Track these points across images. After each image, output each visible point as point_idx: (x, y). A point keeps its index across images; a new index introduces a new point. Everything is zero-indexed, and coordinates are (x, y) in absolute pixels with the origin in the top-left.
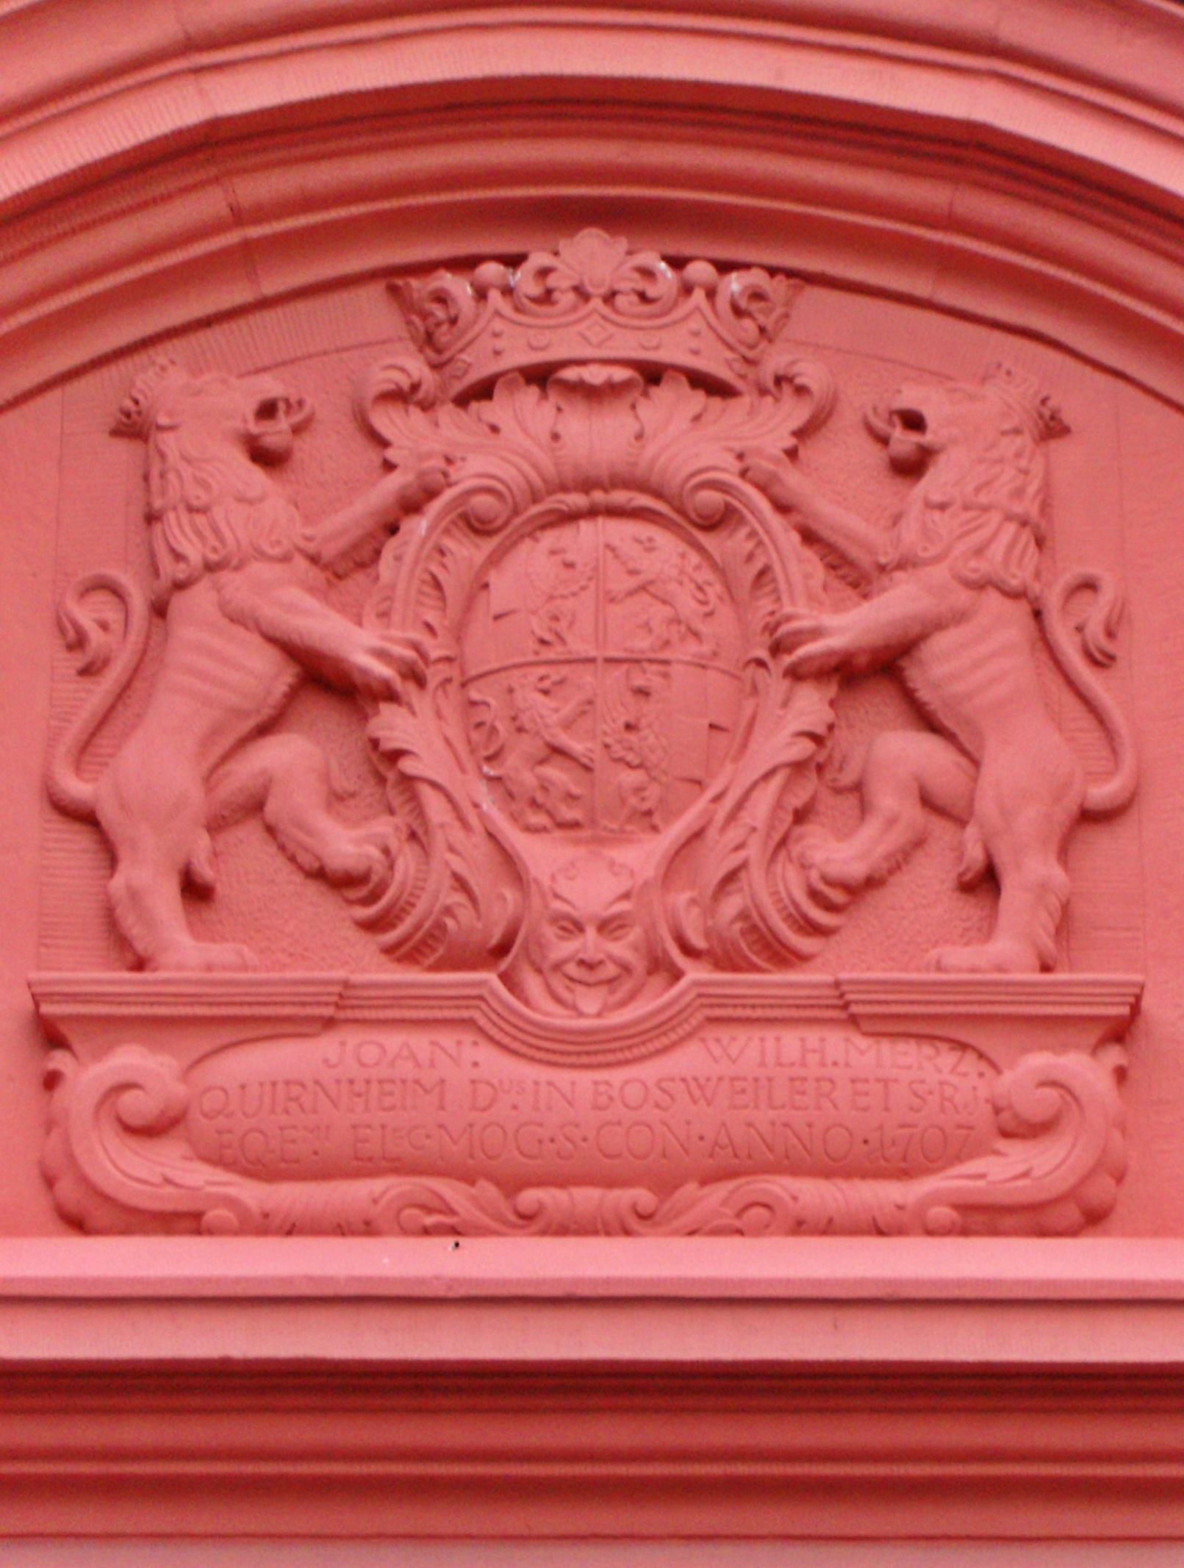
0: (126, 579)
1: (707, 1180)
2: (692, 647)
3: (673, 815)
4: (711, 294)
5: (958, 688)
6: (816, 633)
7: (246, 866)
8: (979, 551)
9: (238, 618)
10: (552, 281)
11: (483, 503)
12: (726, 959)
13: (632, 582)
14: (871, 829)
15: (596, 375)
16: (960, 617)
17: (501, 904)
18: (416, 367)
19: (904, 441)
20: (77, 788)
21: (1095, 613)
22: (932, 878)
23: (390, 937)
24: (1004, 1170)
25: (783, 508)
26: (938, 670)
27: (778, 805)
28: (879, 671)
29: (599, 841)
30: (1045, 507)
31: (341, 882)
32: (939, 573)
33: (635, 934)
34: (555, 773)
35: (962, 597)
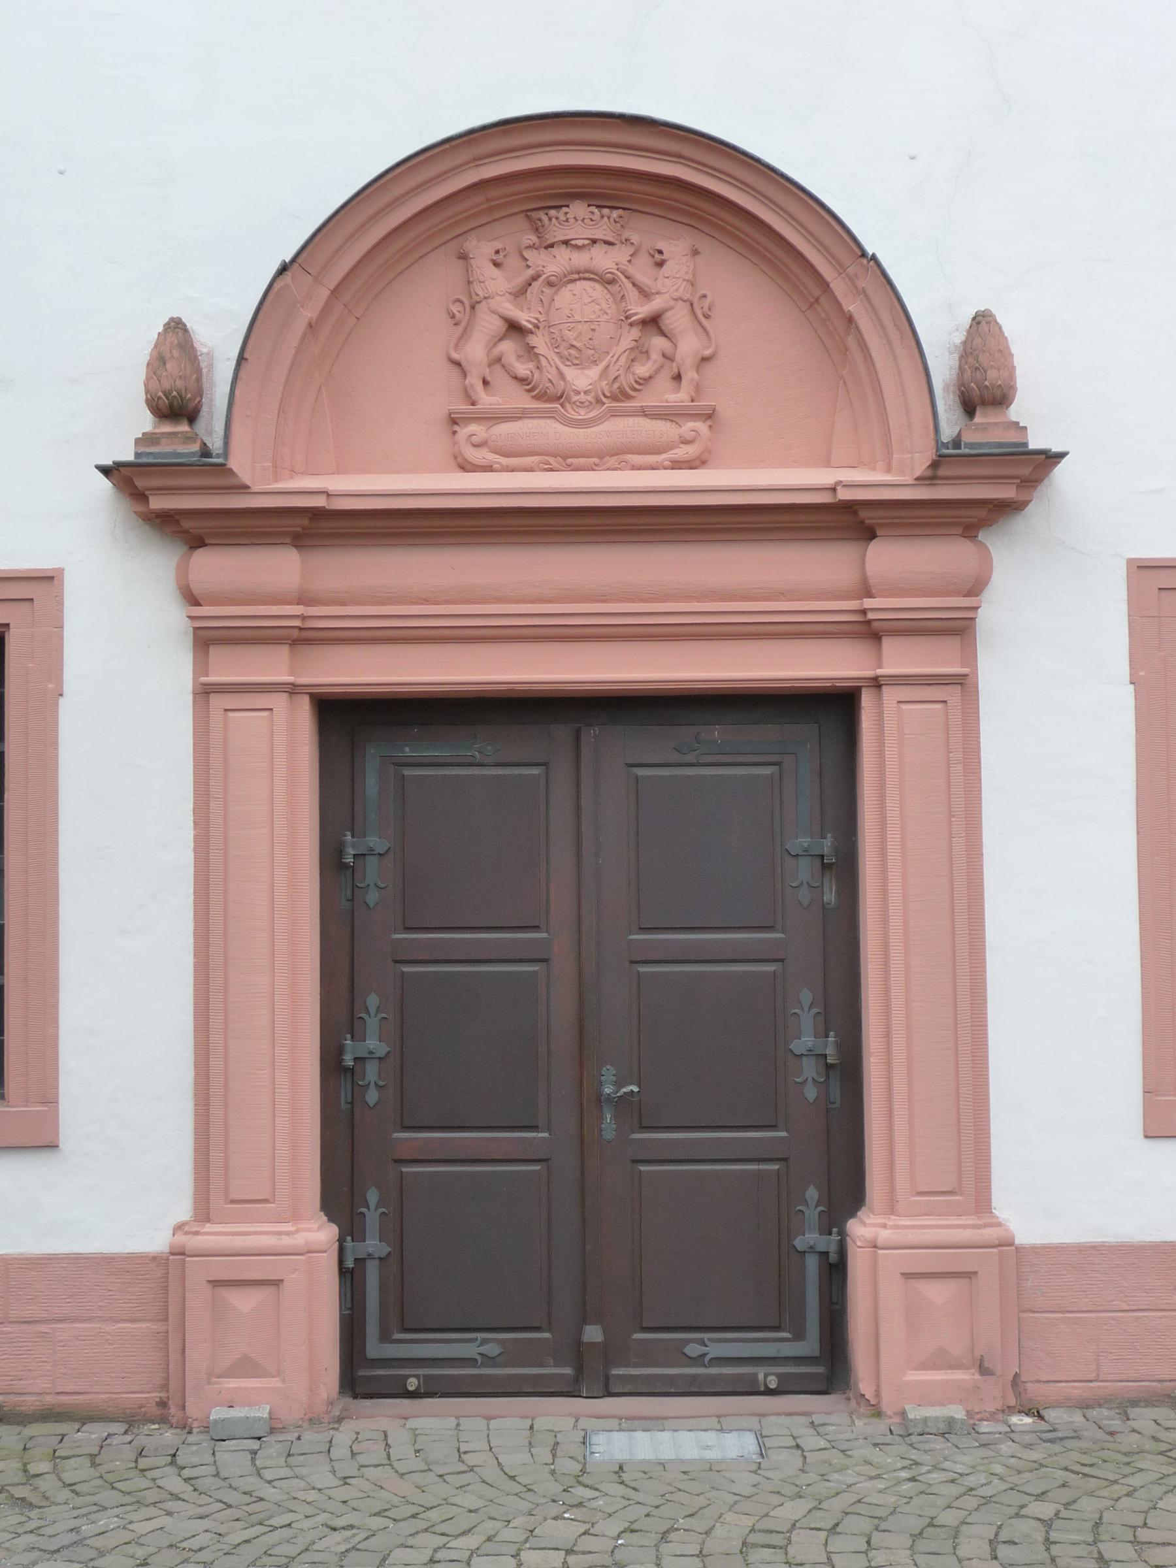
3: (601, 361)
6: (636, 314)
7: (498, 377)
8: (677, 290)
9: (493, 312)
12: (615, 398)
14: (649, 364)
15: (580, 243)
16: (671, 308)
17: (561, 385)
19: (658, 257)
20: (456, 356)
21: (706, 303)
22: (666, 375)
25: (627, 278)
26: (667, 322)
28: (653, 322)
30: (694, 275)
31: (522, 380)
32: (666, 297)
34: (572, 351)
35: (672, 303)
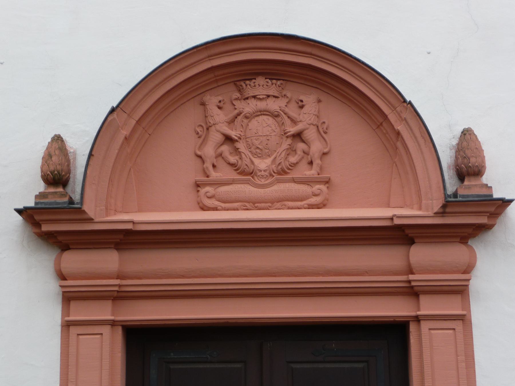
0: (203, 125)
1: (278, 202)
2: (274, 133)
3: (272, 155)
4: (276, 84)
5: (308, 138)
6: (290, 132)
7: (220, 163)
8: (310, 120)
10: (256, 84)
11: (248, 115)
12: (279, 173)
13: (266, 125)
14: (297, 156)
15: (261, 97)
16: (307, 129)
17: (252, 167)
18: (238, 95)
20: (199, 153)
21: (325, 126)
23: (238, 171)
24: (314, 200)
25: (285, 114)
26: (305, 136)
27: (285, 154)
28: (298, 136)
29: (263, 159)
30: (318, 113)
32: (305, 123)
33: (268, 171)
34: (258, 151)
35: (308, 126)
